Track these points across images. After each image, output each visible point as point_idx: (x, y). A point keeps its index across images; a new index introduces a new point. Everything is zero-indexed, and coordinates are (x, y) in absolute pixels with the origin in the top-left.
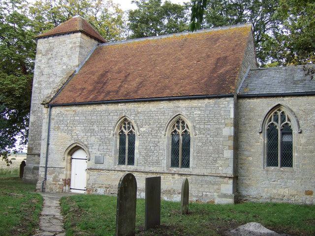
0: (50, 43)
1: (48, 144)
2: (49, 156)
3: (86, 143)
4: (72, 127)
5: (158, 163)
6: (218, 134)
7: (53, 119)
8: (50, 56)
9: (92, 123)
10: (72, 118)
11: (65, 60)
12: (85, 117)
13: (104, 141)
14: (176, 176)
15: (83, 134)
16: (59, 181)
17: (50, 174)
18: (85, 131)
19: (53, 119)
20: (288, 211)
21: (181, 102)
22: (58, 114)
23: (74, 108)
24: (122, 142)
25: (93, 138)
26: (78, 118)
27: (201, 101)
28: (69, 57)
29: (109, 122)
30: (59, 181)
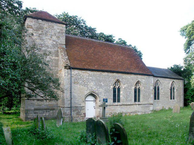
0: (40, 24)
1: (71, 93)
2: (126, 106)
3: (97, 92)
4: (87, 83)
5: (131, 100)
6: (149, 89)
7: (73, 77)
8: (40, 32)
9: (100, 81)
10: (87, 78)
11: (54, 38)
12: (96, 78)
13: (106, 91)
14: (137, 106)
15: (94, 87)
16: (81, 114)
17: (74, 111)
18: (96, 85)
19: (73, 77)
20: (43, 105)
21: (139, 75)
22: (77, 74)
23: (89, 72)
24: (114, 92)
25: (101, 90)
26: (91, 78)
27: (145, 76)
28: (58, 37)
29: (109, 82)
30: (81, 114)
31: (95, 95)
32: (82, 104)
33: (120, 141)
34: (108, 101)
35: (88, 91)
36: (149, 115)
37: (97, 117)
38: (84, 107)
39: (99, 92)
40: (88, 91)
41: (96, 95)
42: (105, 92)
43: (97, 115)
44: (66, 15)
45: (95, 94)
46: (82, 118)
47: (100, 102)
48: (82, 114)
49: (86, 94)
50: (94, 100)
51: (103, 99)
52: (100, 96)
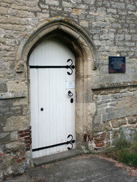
3: (84, 24)
16: (7, 140)
30: (7, 140)
31: (75, 40)
32: (11, 85)
33: (61, 27)
34: (128, 66)
35: (41, 16)
36: (66, 152)
37: (82, 138)
38: (23, 102)
39: (94, 24)
40: (44, 17)
41: (82, 40)
42: (117, 29)
43: (82, 131)
44: (118, 144)
45: (76, 35)
46: (10, 157)
47: (97, 72)
48: (15, 135)
49: (31, 29)
50: (69, 64)
51: (111, 59)
52: (96, 43)
